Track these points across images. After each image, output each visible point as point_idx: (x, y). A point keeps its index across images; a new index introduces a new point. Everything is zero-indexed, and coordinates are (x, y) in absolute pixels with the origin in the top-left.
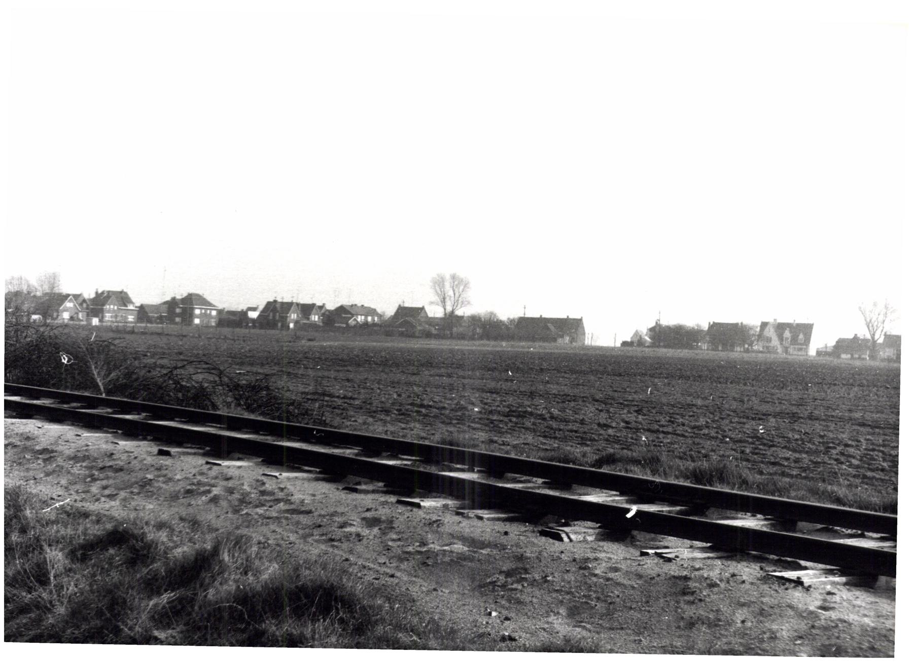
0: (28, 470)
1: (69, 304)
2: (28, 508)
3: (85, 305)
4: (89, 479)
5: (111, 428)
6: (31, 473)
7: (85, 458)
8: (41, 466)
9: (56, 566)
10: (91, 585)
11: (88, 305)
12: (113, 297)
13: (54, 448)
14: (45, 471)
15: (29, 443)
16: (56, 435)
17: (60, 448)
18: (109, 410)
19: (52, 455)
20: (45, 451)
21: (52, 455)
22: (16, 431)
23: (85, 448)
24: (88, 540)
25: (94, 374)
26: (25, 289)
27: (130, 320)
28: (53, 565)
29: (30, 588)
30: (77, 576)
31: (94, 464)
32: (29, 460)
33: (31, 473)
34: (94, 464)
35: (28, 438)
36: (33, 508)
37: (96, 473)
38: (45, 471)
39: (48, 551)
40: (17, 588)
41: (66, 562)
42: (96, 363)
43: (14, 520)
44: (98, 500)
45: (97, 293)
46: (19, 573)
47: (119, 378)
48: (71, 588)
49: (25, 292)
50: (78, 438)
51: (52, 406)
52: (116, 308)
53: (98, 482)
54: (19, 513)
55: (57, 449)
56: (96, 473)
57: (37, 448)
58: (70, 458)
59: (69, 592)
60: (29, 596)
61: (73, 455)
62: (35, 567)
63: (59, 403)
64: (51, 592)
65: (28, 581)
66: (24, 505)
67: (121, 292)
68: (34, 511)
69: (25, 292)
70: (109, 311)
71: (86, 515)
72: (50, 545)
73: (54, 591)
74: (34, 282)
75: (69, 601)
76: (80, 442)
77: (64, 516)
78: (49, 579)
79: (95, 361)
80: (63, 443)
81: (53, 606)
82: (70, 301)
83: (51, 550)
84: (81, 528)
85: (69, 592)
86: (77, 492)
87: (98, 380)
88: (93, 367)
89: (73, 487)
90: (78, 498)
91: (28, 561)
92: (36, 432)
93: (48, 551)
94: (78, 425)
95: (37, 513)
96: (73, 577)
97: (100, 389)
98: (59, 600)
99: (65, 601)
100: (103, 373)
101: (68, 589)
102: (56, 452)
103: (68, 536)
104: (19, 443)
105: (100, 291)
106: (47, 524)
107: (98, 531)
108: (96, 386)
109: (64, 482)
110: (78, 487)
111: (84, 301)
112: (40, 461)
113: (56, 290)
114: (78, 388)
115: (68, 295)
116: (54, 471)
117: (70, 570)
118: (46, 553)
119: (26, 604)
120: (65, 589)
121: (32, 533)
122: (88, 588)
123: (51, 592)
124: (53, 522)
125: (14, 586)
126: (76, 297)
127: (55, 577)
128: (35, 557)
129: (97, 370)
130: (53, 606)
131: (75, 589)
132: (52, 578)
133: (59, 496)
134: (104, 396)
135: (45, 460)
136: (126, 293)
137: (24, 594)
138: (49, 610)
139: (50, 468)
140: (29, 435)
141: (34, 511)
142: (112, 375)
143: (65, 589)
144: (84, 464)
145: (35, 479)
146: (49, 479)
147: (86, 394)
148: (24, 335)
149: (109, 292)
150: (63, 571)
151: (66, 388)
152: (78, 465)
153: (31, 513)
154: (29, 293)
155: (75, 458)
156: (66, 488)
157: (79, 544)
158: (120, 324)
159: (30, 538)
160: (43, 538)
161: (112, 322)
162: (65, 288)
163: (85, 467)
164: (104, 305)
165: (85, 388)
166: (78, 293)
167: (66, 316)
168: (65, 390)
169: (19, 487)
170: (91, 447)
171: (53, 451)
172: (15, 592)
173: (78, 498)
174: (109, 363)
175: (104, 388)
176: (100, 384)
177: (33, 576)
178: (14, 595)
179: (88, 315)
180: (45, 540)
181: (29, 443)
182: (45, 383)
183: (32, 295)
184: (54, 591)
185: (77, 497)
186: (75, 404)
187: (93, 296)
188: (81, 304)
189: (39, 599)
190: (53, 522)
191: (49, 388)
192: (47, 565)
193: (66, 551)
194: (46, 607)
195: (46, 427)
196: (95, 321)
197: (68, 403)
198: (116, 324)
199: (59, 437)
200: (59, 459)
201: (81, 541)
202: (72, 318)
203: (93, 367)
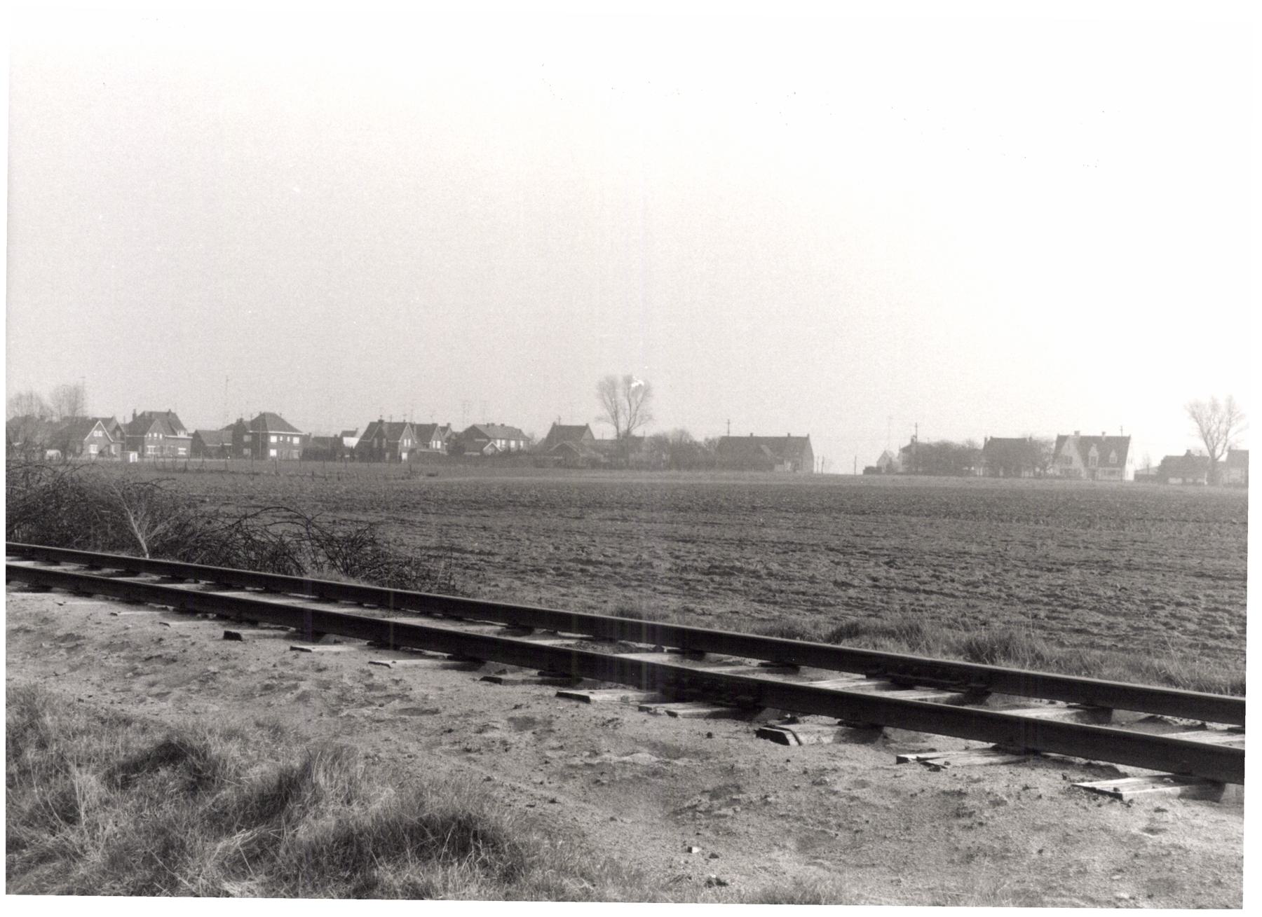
0: (46, 663)
1: (98, 434)
2: (47, 713)
3: (118, 434)
4: (130, 674)
5: (158, 603)
6: (51, 668)
7: (125, 645)
8: (64, 658)
9: (87, 797)
10: (136, 823)
11: (122, 434)
12: (157, 422)
13: (82, 633)
14: (69, 665)
15: (46, 628)
16: (84, 615)
17: (89, 633)
18: (156, 578)
19: (78, 642)
20: (69, 637)
21: (78, 642)
22: (29, 609)
23: (123, 633)
24: (130, 758)
25: (133, 528)
26: (36, 412)
27: (180, 453)
28: (84, 796)
29: (54, 828)
30: (117, 810)
31: (136, 653)
32: (47, 650)
33: (51, 668)
34: (136, 653)
35: (45, 620)
36: (55, 714)
37: (140, 666)
38: (69, 665)
39: (77, 774)
40: (36, 828)
41: (102, 790)
42: (136, 513)
43: (30, 731)
44: (142, 701)
45: (134, 415)
46: (38, 807)
47: (168, 531)
48: (108, 828)
49: (37, 416)
50: (114, 618)
51: (77, 573)
52: (161, 436)
53: (143, 677)
54: (36, 721)
55: (85, 634)
56: (140, 666)
57: (59, 633)
58: (104, 647)
59: (107, 832)
60: (53, 839)
61: (107, 642)
62: (59, 799)
63: (87, 568)
64: (82, 833)
65: (51, 819)
66: (42, 710)
67: (168, 413)
68: (56, 718)
69: (37, 416)
70: (152, 442)
71: (127, 722)
72: (79, 765)
73: (86, 832)
74: (47, 400)
75: (107, 845)
76: (117, 623)
77: (97, 724)
78: (79, 815)
79: (133, 511)
80: (94, 626)
81: (85, 852)
82: (99, 428)
83: (81, 773)
84: (120, 740)
85: (107, 832)
86: (114, 690)
87: (139, 537)
88: (132, 518)
89: (109, 684)
90: (116, 699)
91: (50, 788)
92: (57, 611)
93: (77, 774)
94: (113, 600)
95: (60, 720)
96: (110, 812)
97: (142, 549)
98: (93, 844)
99: (101, 845)
100: (145, 527)
101: (104, 829)
102: (84, 638)
103: (104, 752)
104: (33, 627)
105: (139, 413)
106: (74, 734)
107: (144, 743)
108: (136, 545)
109: (96, 678)
110: (114, 684)
111: (118, 428)
112: (62, 652)
113: (79, 414)
114: (112, 547)
115: (95, 420)
116: (82, 664)
117: (107, 802)
118: (74, 777)
119: (49, 850)
120: (101, 828)
121: (55, 748)
122: (132, 827)
123: (82, 833)
124: (82, 732)
125: (31, 825)
126: (107, 421)
127: (86, 812)
128: (59, 784)
129: (138, 523)
130: (85, 852)
131: (115, 828)
132: (83, 814)
133: (90, 696)
134: (147, 557)
135: (69, 650)
136: (174, 415)
137: (46, 836)
138: (79, 857)
139: (76, 660)
140: (47, 615)
141: (56, 718)
142: (158, 528)
143: (101, 828)
144: (123, 654)
145: (56, 675)
146: (76, 674)
147: (124, 555)
148: (37, 477)
149: (151, 413)
150: (98, 803)
151: (96, 547)
152: (115, 655)
153: (52, 720)
154: (42, 418)
155: (110, 646)
156: (98, 686)
157: (118, 763)
158: (167, 460)
159: (52, 756)
160: (69, 755)
161: (156, 457)
162: (95, 408)
163: (124, 658)
164: (144, 433)
165: (122, 547)
166: (109, 416)
167: (93, 450)
168: (94, 550)
169: (35, 686)
170: (131, 631)
171: (79, 638)
172: (33, 833)
173: (116, 699)
174: (153, 514)
175: (148, 548)
176: (142, 541)
177: (57, 811)
178: (32, 838)
179: (123, 448)
180: (72, 759)
181: (46, 628)
182: (67, 541)
183: (47, 420)
184: (86, 832)
185: (113, 698)
186: (107, 571)
187: (129, 420)
188: (113, 433)
189: (66, 843)
190: (82, 732)
191: (73, 548)
192: (75, 794)
193: (101, 774)
194: (75, 853)
195: (69, 603)
196: (133, 457)
197: (98, 568)
198: (162, 460)
199: (88, 618)
200: (88, 648)
201: (122, 759)
202: (101, 453)
203: (132, 518)
